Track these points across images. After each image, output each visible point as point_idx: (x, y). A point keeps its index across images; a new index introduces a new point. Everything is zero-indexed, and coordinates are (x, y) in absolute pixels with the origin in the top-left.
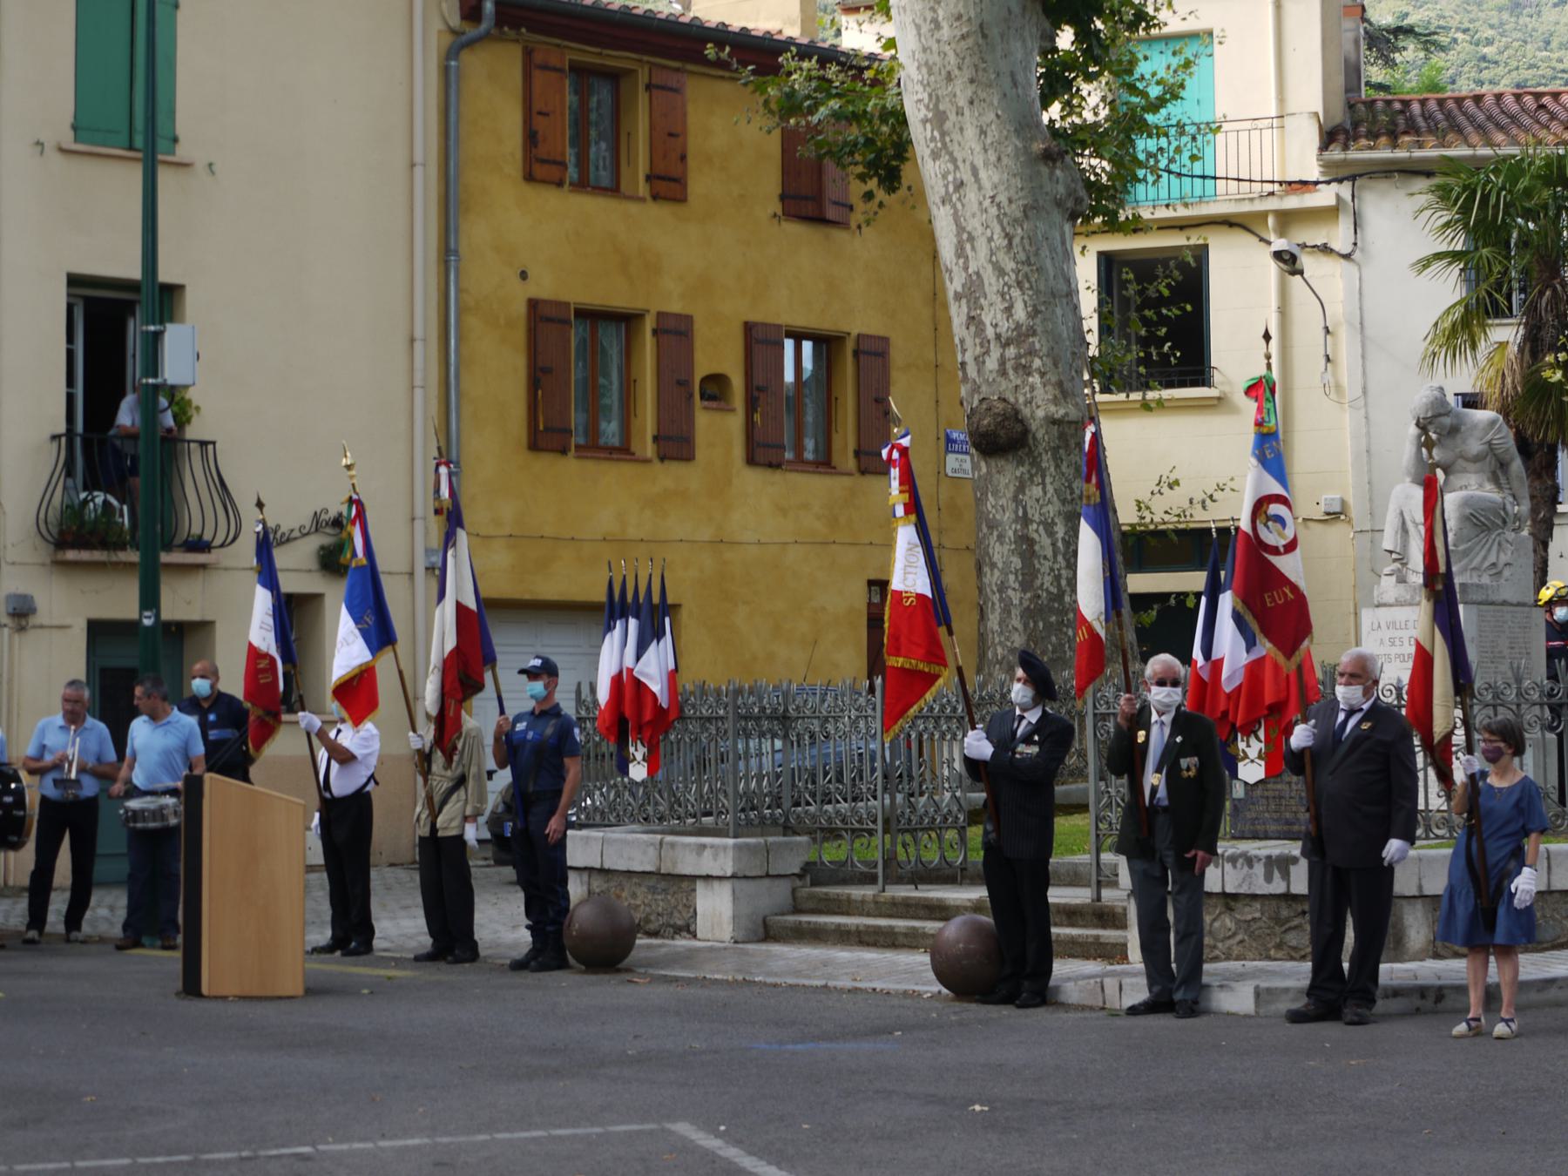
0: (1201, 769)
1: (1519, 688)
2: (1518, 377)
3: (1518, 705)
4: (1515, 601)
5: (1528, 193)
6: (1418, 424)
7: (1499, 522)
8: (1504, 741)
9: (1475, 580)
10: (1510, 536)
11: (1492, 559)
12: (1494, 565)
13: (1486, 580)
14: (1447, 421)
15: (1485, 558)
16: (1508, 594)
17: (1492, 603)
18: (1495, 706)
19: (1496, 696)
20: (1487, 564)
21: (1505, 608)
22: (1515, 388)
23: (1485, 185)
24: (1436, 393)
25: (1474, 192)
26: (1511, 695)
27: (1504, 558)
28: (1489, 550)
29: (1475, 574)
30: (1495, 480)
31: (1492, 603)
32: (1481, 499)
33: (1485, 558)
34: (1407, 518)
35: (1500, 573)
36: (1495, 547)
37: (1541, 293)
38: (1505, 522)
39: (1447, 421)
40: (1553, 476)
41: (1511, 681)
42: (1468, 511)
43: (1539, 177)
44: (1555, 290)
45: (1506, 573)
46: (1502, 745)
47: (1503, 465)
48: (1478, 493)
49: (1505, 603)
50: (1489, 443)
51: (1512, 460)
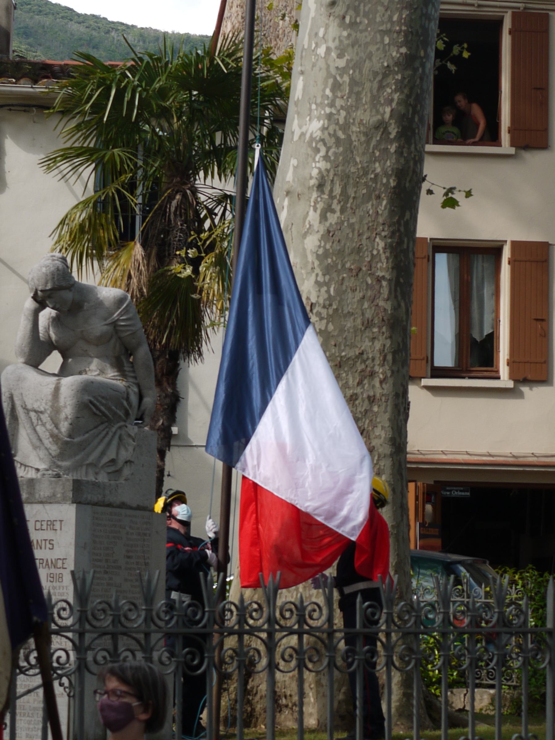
0: (170, 595)
1: (149, 611)
2: (144, 279)
3: (147, 635)
4: (134, 505)
5: (163, 93)
6: (35, 297)
7: (121, 413)
8: (139, 697)
9: (91, 478)
10: (133, 430)
11: (111, 454)
12: (113, 461)
13: (103, 478)
14: (68, 295)
15: (103, 453)
16: (126, 495)
17: (110, 505)
18: (114, 636)
19: (116, 620)
20: (105, 460)
21: (124, 511)
22: (141, 290)
23: (120, 81)
24: (59, 263)
25: (109, 89)
26: (137, 621)
27: (124, 455)
28: (109, 444)
29: (91, 471)
30: (118, 365)
31: (110, 505)
32: (102, 385)
33: (103, 453)
34: (18, 403)
35: (119, 472)
36: (115, 442)
37: (171, 198)
38: (127, 414)
39: (68, 295)
40: (174, 384)
41: (140, 602)
42: (87, 398)
43: (176, 78)
44: (185, 195)
45: (126, 472)
46: (135, 703)
47: (128, 351)
48: (100, 378)
49: (123, 505)
50: (114, 324)
51: (139, 344)
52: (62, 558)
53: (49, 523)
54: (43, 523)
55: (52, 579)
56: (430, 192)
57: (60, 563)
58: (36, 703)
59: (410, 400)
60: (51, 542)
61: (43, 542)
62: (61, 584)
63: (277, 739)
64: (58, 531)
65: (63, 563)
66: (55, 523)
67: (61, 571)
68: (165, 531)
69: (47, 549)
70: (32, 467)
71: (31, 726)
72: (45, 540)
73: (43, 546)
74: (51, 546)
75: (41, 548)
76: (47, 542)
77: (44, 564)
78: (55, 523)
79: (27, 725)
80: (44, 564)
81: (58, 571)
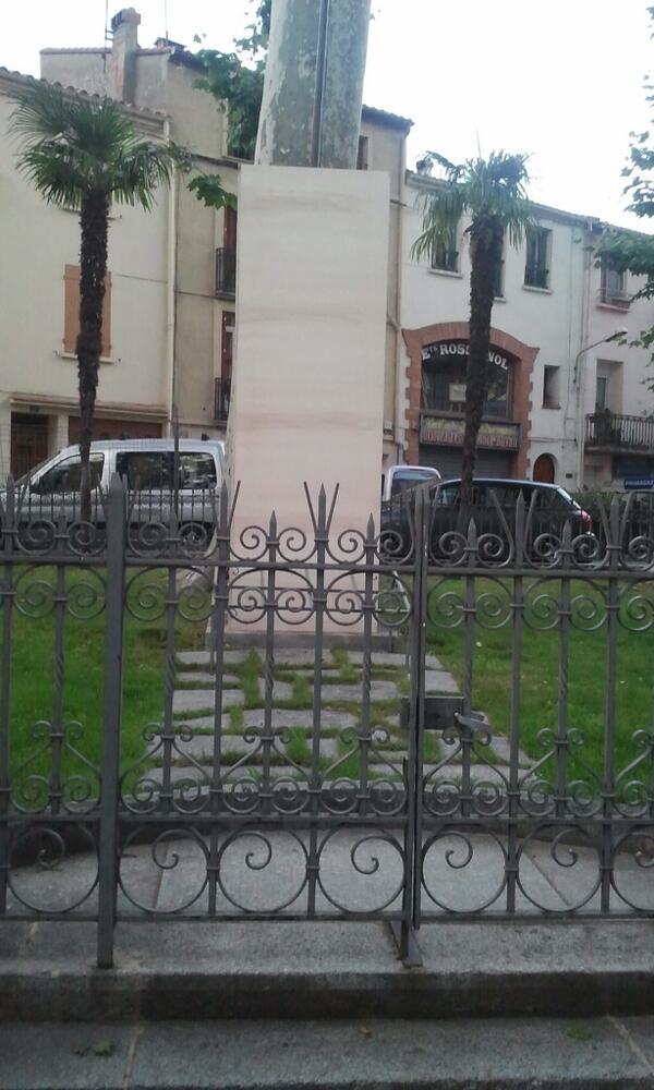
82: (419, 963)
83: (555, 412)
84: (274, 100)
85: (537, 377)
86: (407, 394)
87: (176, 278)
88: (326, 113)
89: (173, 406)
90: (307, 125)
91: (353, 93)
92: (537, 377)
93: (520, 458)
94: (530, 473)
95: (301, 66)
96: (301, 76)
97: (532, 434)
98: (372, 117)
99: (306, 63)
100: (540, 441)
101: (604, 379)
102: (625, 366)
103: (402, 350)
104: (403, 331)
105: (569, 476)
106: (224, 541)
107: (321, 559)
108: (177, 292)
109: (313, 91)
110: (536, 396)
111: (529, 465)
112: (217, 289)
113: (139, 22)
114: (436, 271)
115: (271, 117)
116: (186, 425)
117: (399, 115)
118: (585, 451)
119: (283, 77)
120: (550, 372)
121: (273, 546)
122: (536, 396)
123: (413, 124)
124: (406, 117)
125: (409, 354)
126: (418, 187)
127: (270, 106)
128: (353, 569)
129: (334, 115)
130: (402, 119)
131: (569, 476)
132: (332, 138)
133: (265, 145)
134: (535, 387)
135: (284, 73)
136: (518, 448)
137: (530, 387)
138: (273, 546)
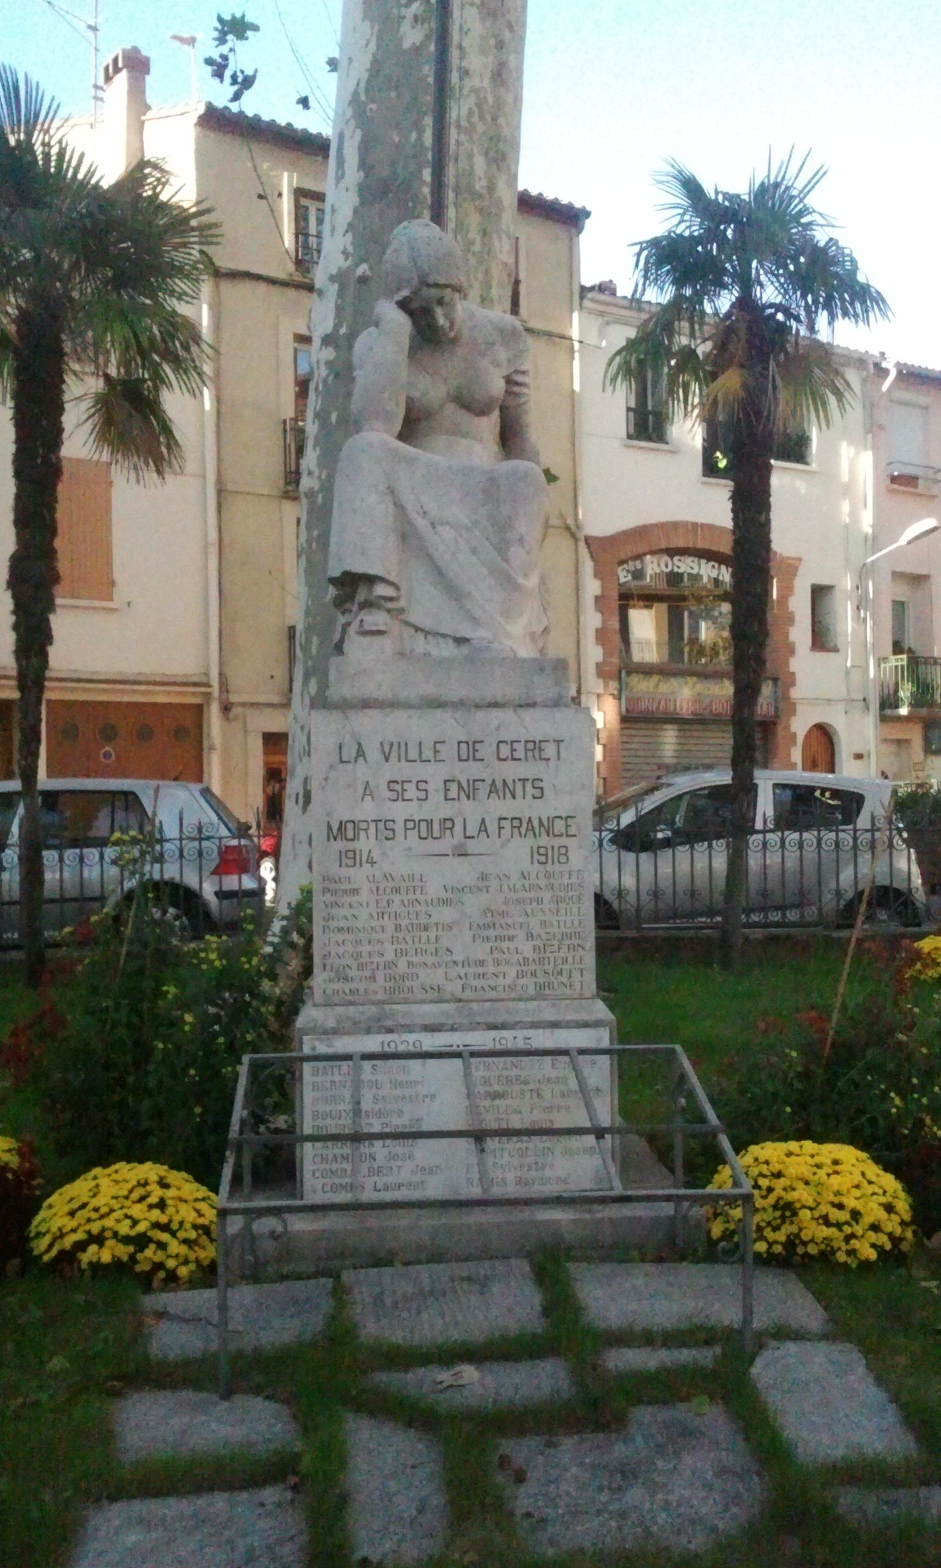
52: (564, 815)
53: (410, 825)
54: (515, 745)
55: (543, 859)
56: (437, 791)
57: (559, 826)
58: (535, 1112)
59: (9, 594)
60: (538, 784)
61: (519, 785)
62: (564, 868)
63: (303, 78)
64: (552, 764)
65: (567, 826)
66: (543, 745)
67: (565, 841)
68: (617, 586)
69: (529, 797)
70: (444, 636)
71: (529, 1160)
72: (524, 781)
73: (519, 792)
74: (538, 793)
75: (514, 796)
76: (529, 785)
77: (523, 830)
78: (543, 745)
79: (516, 1161)
80: (523, 830)
81: (557, 842)
82: (240, 155)
83: (832, 655)
84: (356, 94)
85: (800, 605)
86: (597, 638)
87: (219, 459)
88: (457, 111)
89: (220, 674)
90: (421, 132)
91: (502, 152)
92: (800, 605)
93: (780, 732)
94: (796, 755)
95: (406, 27)
96: (406, 45)
97: (795, 693)
98: (533, 206)
99: (416, 18)
100: (814, 702)
101: (902, 604)
102: (933, 580)
103: (588, 566)
104: (587, 540)
105: (859, 756)
106: (607, 928)
107: (855, 833)
108: (220, 492)
109: (428, 71)
110: (800, 633)
111: (795, 743)
112: (287, 484)
113: (148, 72)
114: (635, 443)
115: (353, 122)
116: (243, 704)
117: (565, 201)
118: (881, 715)
119: (373, 46)
120: (819, 593)
121: (200, 830)
122: (800, 633)
123: (587, 214)
124: (578, 205)
125: (597, 574)
126: (602, 314)
127: (350, 103)
128: (193, 839)
129: (470, 113)
130: (570, 207)
131: (859, 756)
132: (470, 157)
133: (343, 176)
134: (797, 618)
135: (374, 40)
136: (777, 716)
137: (790, 619)
138: (200, 830)
